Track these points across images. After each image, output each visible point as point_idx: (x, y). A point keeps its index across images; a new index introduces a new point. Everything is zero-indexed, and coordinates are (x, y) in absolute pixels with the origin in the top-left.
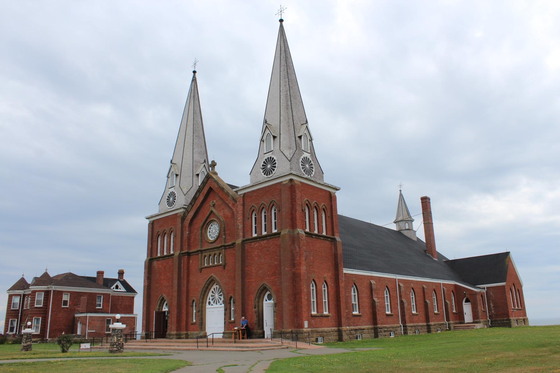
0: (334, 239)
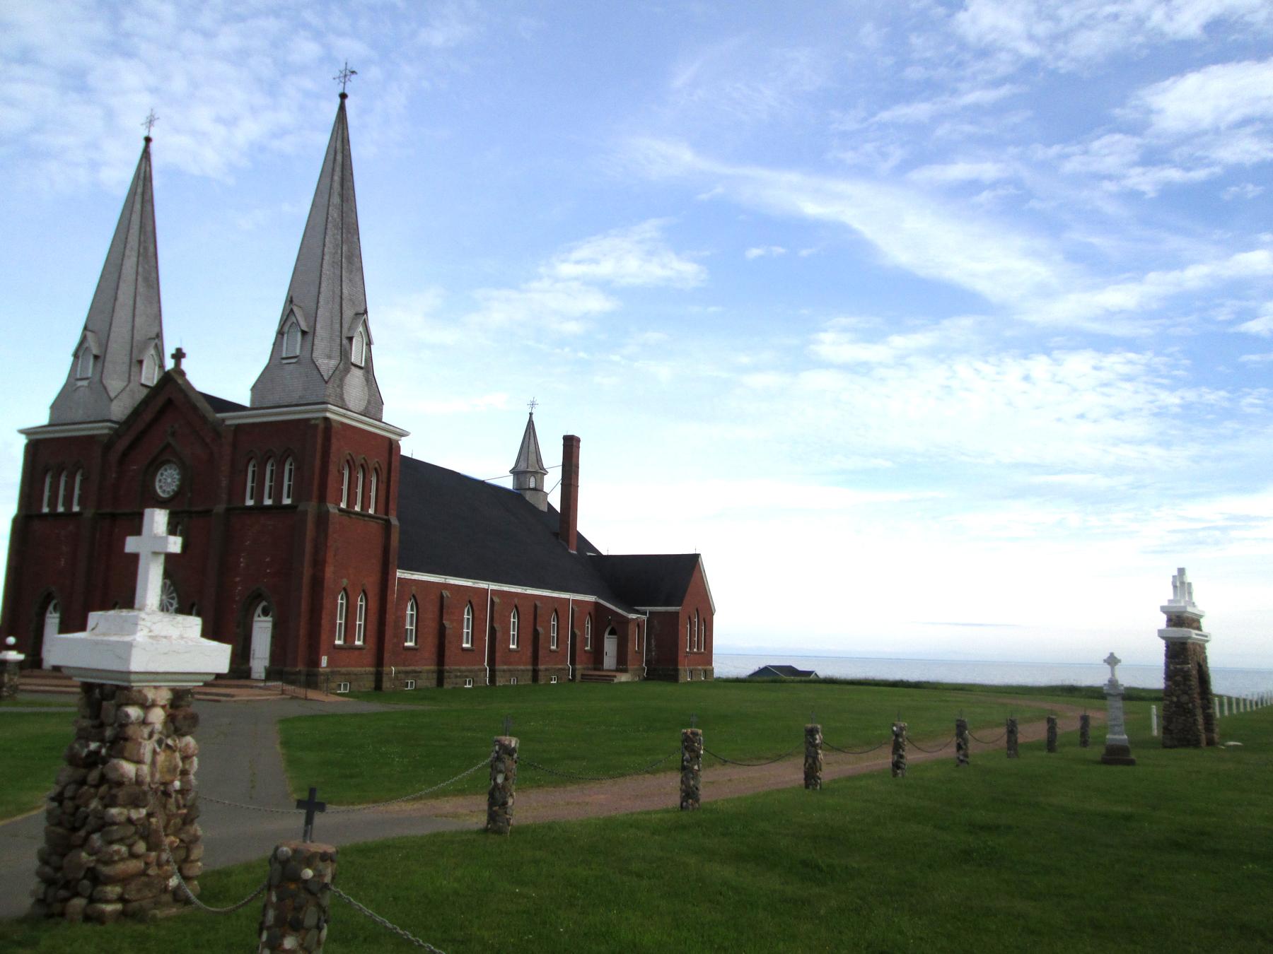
0: (388, 521)
